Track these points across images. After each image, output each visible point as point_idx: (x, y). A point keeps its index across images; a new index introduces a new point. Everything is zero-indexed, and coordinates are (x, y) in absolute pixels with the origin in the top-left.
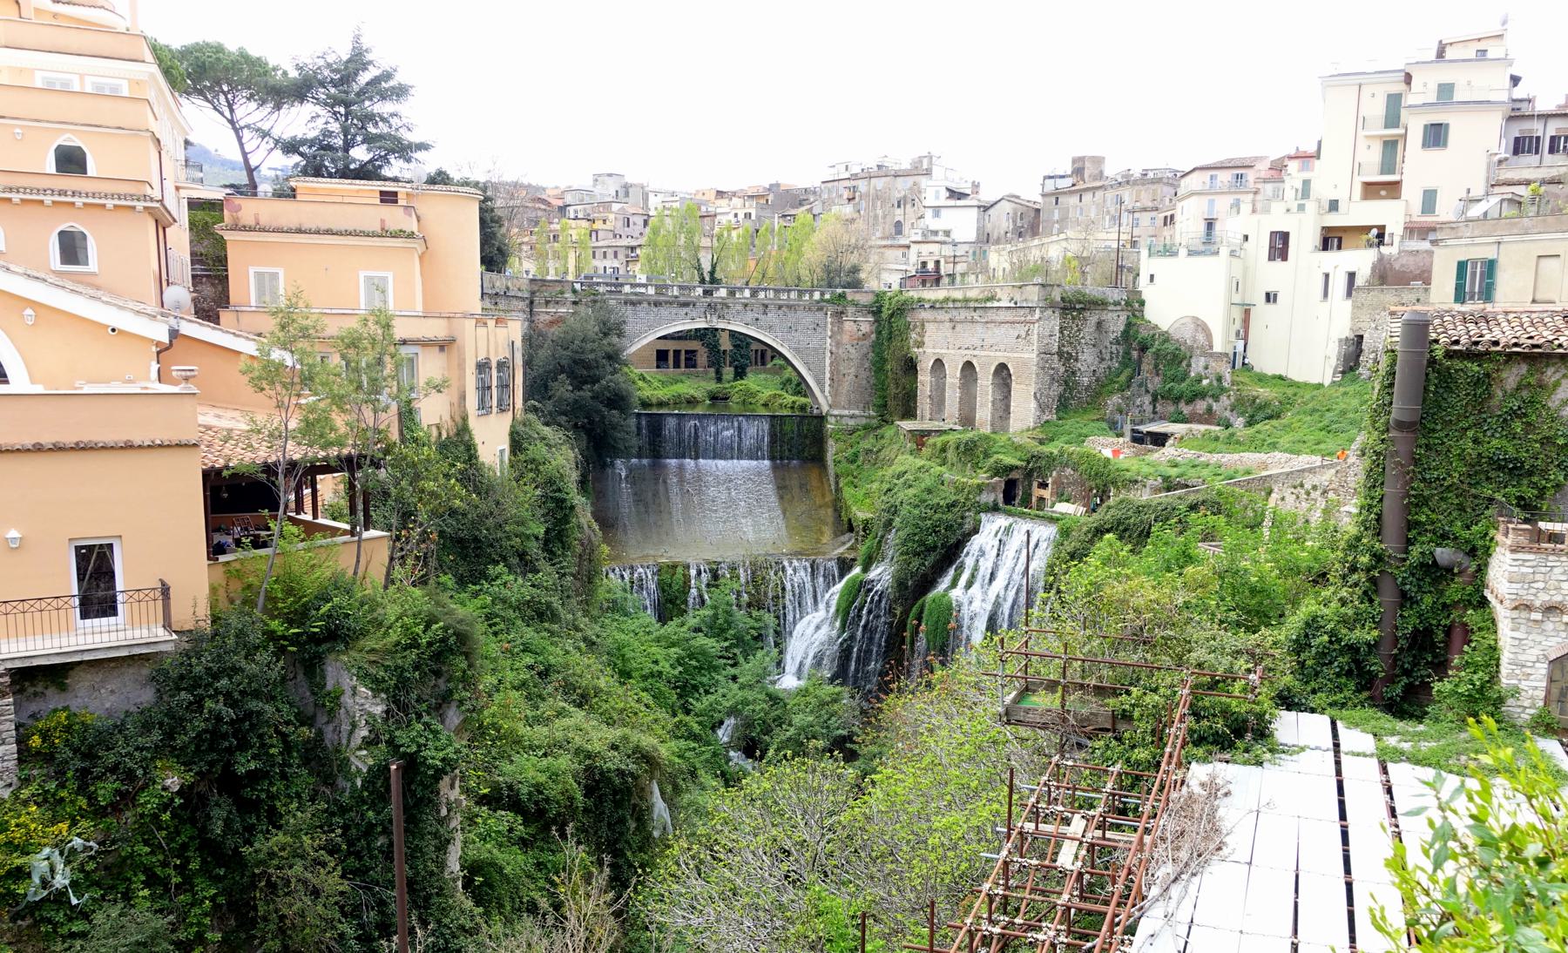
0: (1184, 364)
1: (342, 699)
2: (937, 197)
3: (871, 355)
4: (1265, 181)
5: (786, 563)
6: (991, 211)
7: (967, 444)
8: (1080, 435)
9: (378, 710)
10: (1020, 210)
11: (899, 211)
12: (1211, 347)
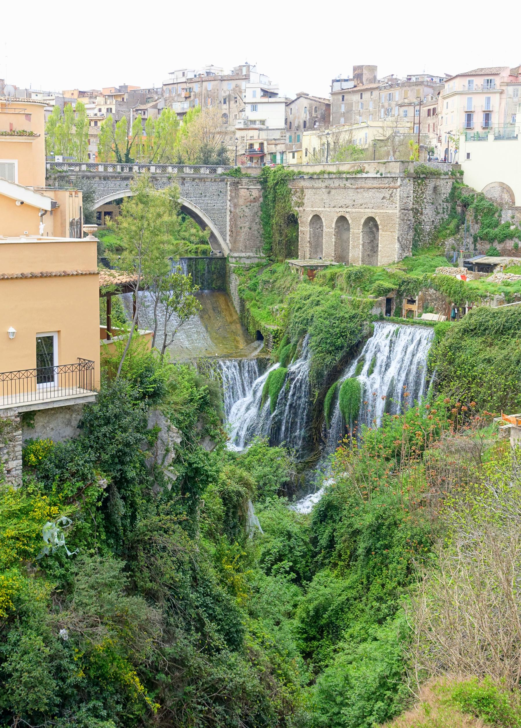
0: (496, 215)
1: (159, 434)
2: (254, 96)
3: (260, 213)
4: (508, 84)
5: (222, 364)
6: (292, 106)
7: (356, 274)
8: (431, 266)
9: (179, 440)
10: (315, 104)
11: (225, 106)
12: (514, 203)
